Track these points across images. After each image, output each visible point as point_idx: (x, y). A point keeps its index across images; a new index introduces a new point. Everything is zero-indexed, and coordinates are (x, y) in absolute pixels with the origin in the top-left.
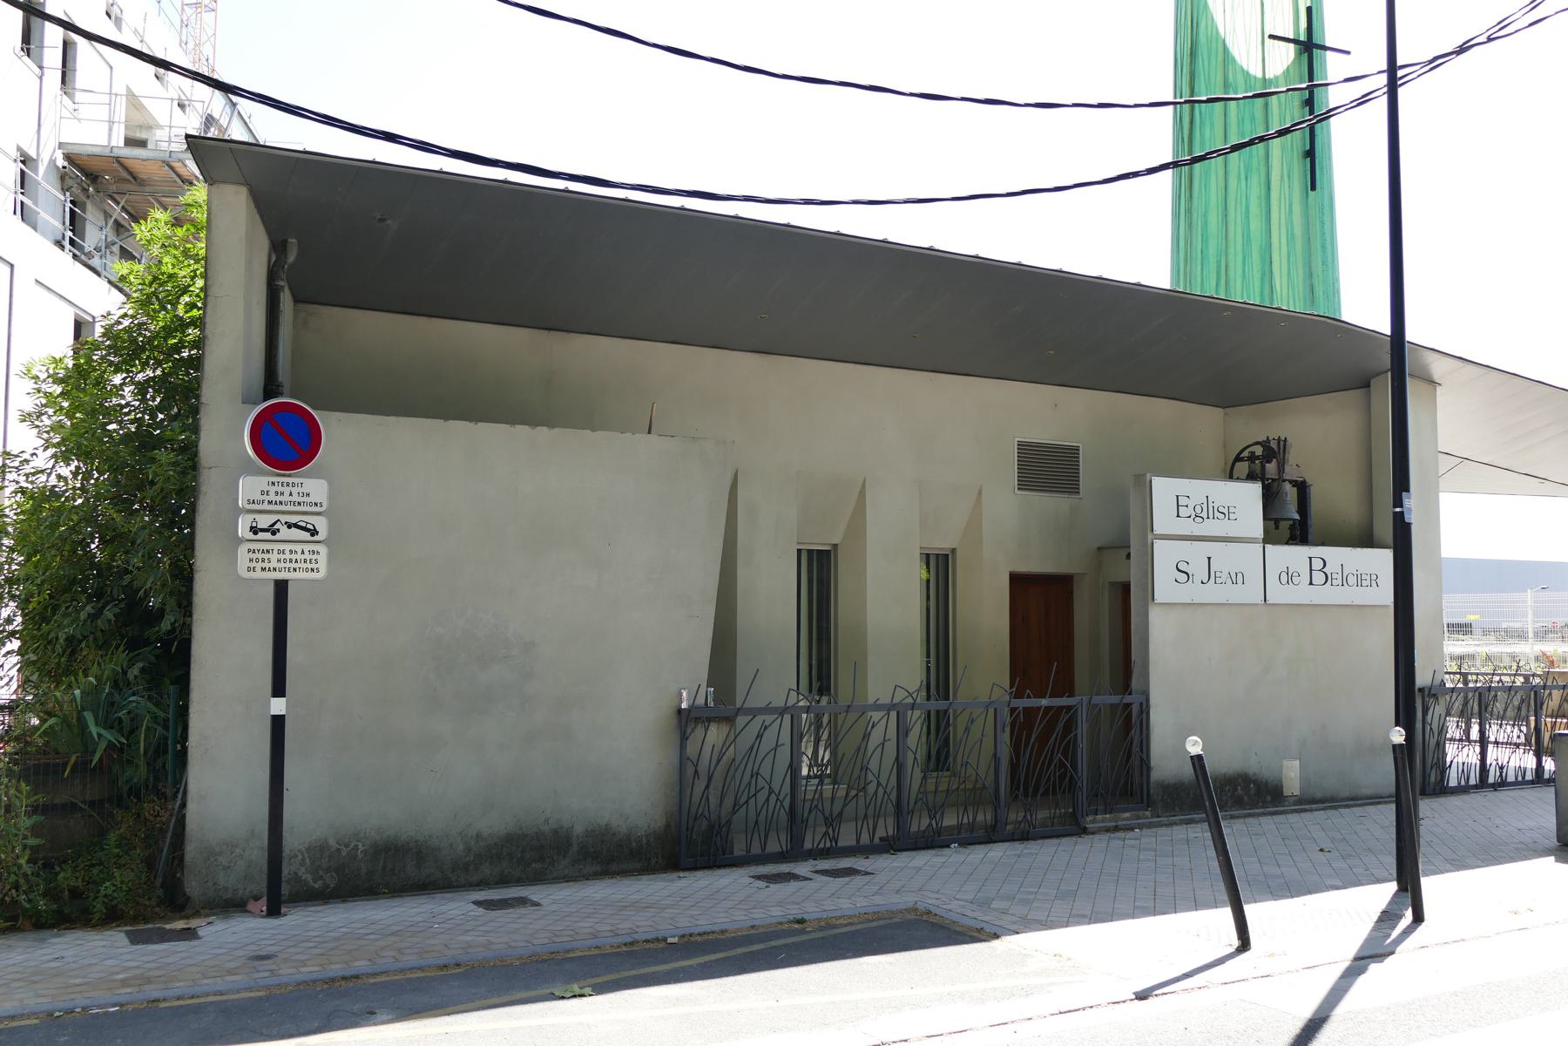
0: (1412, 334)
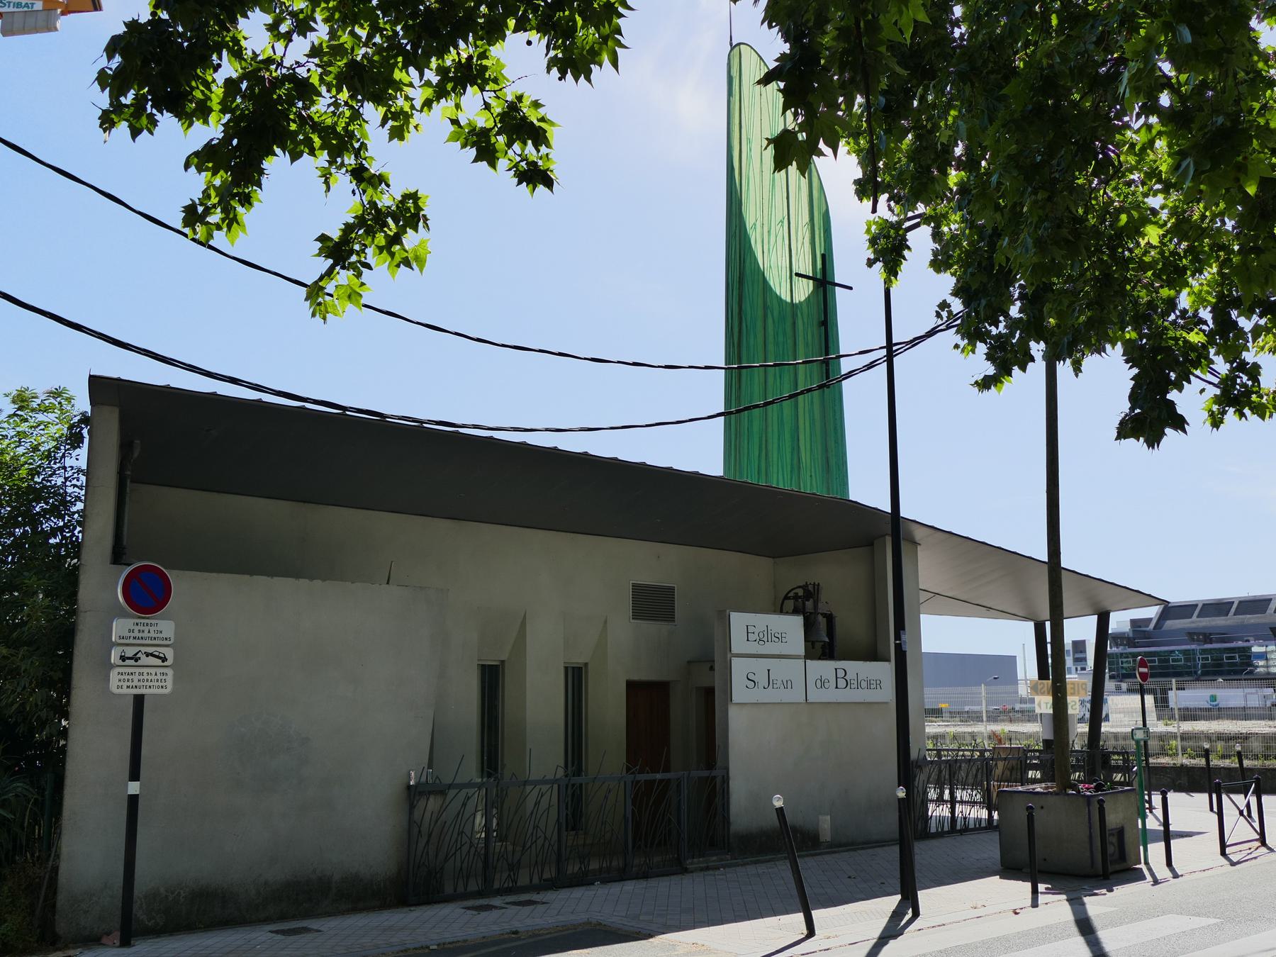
0: (905, 512)
